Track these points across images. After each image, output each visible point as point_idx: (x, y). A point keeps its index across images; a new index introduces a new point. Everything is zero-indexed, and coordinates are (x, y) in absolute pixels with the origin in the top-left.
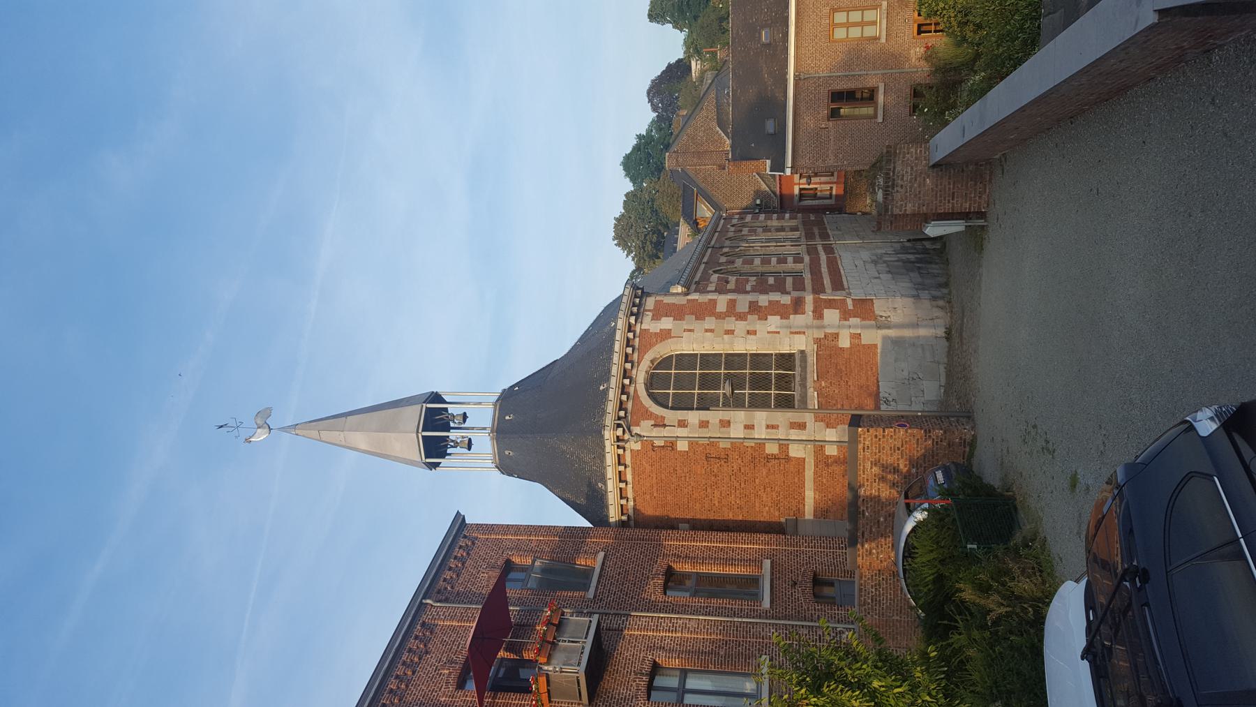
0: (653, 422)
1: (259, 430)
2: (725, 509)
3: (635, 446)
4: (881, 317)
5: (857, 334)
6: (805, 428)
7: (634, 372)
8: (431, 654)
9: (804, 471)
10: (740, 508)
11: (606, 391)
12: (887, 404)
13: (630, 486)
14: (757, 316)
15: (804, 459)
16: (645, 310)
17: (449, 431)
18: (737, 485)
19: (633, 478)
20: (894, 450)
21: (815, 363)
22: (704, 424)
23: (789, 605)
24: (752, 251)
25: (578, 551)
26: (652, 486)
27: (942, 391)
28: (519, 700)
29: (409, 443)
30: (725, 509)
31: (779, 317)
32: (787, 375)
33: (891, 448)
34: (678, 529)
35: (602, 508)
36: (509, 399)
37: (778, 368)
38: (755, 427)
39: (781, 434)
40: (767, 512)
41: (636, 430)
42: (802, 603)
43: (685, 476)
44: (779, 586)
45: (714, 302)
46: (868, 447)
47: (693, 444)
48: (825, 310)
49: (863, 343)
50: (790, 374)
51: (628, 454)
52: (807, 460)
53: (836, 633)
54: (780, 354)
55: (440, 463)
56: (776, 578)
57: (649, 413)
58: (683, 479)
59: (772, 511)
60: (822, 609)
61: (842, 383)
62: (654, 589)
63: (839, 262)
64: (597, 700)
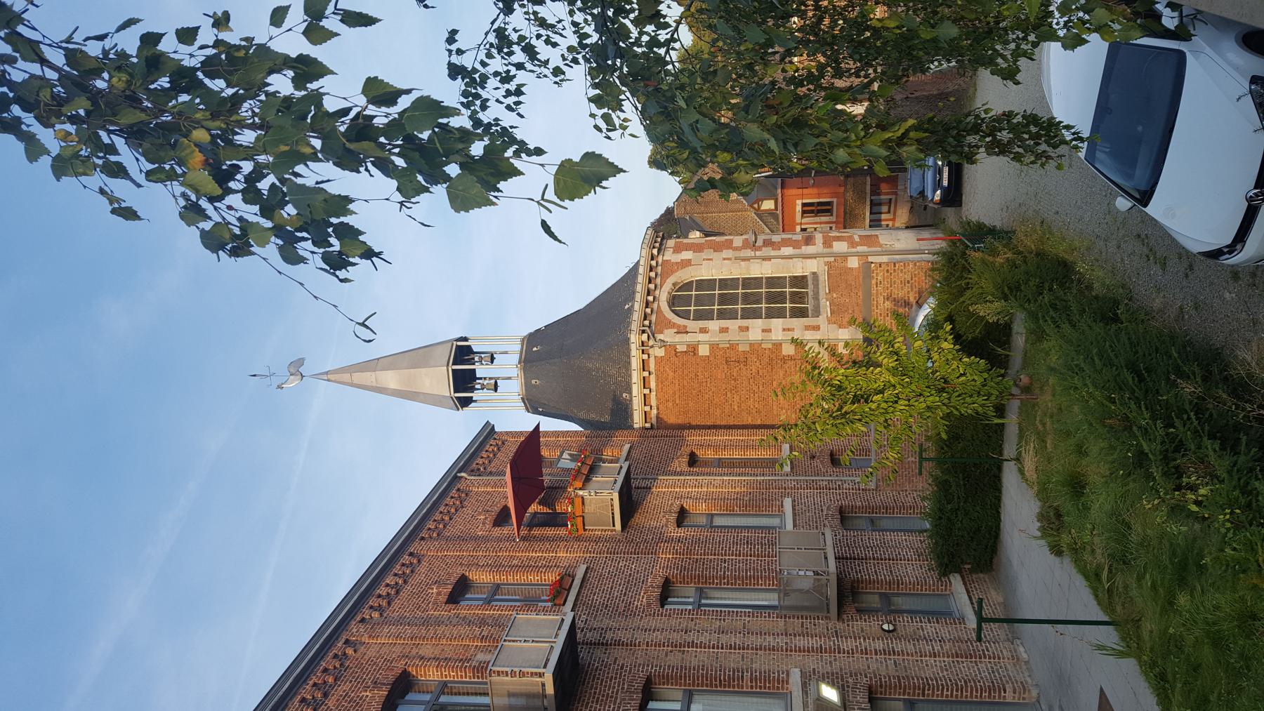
0: (676, 330)
1: (292, 377)
2: (744, 414)
3: (660, 352)
7: (657, 292)
10: (758, 412)
11: (631, 310)
13: (654, 394)
18: (755, 388)
19: (657, 386)
22: (724, 330)
25: (605, 445)
26: (674, 393)
29: (439, 379)
30: (744, 414)
32: (800, 293)
35: (626, 419)
36: (533, 338)
37: (791, 287)
41: (659, 337)
45: (731, 241)
47: (714, 347)
51: (652, 361)
58: (704, 384)
62: (681, 463)
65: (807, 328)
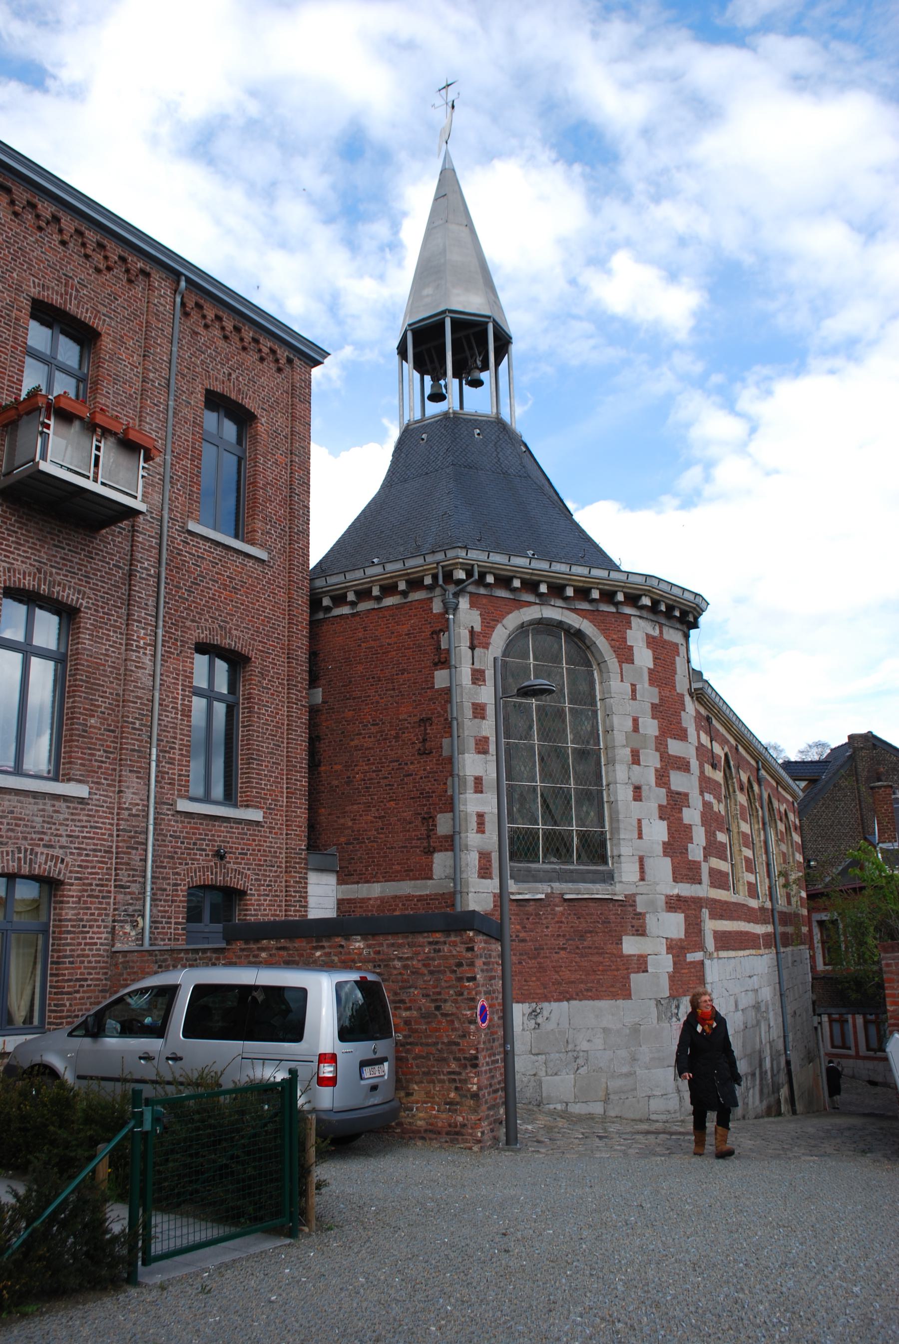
0: (478, 628)
4: (678, 1007)
5: (646, 967)
6: (483, 877)
8: (94, 275)
9: (411, 879)
12: (530, 1014)
14: (664, 803)
15: (431, 878)
16: (661, 625)
17: (454, 376)
20: (436, 1000)
21: (593, 896)
22: (479, 711)
23: (182, 843)
24: (756, 827)
27: (559, 1107)
28: (8, 386)
31: (666, 840)
33: (439, 993)
34: (310, 688)
38: (479, 795)
39: (472, 838)
40: (343, 825)
42: (187, 864)
43: (394, 689)
44: (216, 831)
45: (682, 736)
46: (439, 951)
48: (683, 915)
49: (633, 976)
50: (572, 856)
52: (430, 882)
53: (133, 916)
54: (605, 840)
55: (407, 361)
56: (232, 828)
57: (493, 623)
58: (390, 686)
59: (346, 832)
60: (178, 896)
61: (561, 941)
63: (753, 952)
64: (7, 507)
65: (484, 857)
